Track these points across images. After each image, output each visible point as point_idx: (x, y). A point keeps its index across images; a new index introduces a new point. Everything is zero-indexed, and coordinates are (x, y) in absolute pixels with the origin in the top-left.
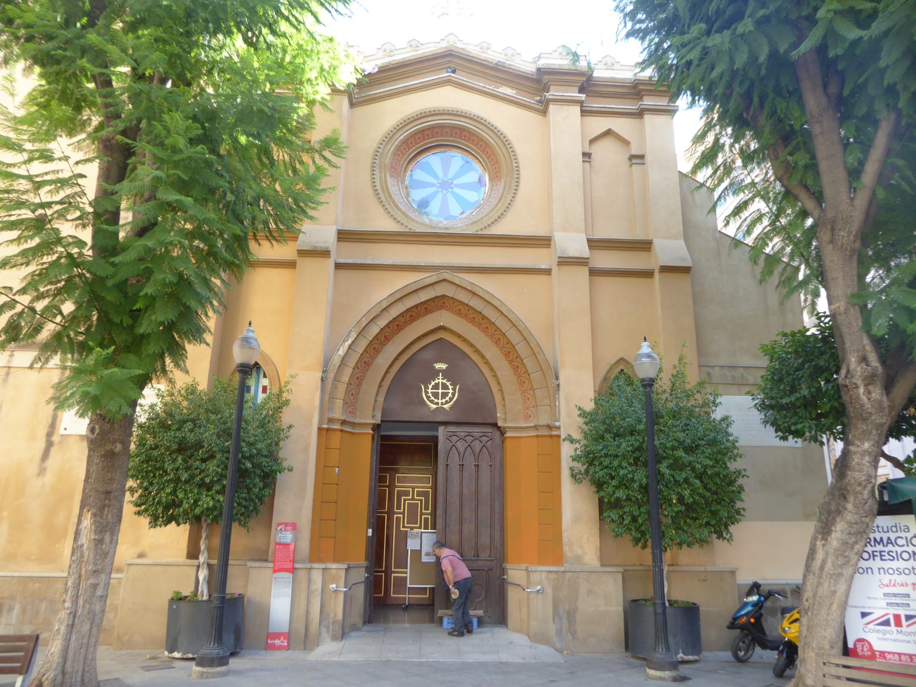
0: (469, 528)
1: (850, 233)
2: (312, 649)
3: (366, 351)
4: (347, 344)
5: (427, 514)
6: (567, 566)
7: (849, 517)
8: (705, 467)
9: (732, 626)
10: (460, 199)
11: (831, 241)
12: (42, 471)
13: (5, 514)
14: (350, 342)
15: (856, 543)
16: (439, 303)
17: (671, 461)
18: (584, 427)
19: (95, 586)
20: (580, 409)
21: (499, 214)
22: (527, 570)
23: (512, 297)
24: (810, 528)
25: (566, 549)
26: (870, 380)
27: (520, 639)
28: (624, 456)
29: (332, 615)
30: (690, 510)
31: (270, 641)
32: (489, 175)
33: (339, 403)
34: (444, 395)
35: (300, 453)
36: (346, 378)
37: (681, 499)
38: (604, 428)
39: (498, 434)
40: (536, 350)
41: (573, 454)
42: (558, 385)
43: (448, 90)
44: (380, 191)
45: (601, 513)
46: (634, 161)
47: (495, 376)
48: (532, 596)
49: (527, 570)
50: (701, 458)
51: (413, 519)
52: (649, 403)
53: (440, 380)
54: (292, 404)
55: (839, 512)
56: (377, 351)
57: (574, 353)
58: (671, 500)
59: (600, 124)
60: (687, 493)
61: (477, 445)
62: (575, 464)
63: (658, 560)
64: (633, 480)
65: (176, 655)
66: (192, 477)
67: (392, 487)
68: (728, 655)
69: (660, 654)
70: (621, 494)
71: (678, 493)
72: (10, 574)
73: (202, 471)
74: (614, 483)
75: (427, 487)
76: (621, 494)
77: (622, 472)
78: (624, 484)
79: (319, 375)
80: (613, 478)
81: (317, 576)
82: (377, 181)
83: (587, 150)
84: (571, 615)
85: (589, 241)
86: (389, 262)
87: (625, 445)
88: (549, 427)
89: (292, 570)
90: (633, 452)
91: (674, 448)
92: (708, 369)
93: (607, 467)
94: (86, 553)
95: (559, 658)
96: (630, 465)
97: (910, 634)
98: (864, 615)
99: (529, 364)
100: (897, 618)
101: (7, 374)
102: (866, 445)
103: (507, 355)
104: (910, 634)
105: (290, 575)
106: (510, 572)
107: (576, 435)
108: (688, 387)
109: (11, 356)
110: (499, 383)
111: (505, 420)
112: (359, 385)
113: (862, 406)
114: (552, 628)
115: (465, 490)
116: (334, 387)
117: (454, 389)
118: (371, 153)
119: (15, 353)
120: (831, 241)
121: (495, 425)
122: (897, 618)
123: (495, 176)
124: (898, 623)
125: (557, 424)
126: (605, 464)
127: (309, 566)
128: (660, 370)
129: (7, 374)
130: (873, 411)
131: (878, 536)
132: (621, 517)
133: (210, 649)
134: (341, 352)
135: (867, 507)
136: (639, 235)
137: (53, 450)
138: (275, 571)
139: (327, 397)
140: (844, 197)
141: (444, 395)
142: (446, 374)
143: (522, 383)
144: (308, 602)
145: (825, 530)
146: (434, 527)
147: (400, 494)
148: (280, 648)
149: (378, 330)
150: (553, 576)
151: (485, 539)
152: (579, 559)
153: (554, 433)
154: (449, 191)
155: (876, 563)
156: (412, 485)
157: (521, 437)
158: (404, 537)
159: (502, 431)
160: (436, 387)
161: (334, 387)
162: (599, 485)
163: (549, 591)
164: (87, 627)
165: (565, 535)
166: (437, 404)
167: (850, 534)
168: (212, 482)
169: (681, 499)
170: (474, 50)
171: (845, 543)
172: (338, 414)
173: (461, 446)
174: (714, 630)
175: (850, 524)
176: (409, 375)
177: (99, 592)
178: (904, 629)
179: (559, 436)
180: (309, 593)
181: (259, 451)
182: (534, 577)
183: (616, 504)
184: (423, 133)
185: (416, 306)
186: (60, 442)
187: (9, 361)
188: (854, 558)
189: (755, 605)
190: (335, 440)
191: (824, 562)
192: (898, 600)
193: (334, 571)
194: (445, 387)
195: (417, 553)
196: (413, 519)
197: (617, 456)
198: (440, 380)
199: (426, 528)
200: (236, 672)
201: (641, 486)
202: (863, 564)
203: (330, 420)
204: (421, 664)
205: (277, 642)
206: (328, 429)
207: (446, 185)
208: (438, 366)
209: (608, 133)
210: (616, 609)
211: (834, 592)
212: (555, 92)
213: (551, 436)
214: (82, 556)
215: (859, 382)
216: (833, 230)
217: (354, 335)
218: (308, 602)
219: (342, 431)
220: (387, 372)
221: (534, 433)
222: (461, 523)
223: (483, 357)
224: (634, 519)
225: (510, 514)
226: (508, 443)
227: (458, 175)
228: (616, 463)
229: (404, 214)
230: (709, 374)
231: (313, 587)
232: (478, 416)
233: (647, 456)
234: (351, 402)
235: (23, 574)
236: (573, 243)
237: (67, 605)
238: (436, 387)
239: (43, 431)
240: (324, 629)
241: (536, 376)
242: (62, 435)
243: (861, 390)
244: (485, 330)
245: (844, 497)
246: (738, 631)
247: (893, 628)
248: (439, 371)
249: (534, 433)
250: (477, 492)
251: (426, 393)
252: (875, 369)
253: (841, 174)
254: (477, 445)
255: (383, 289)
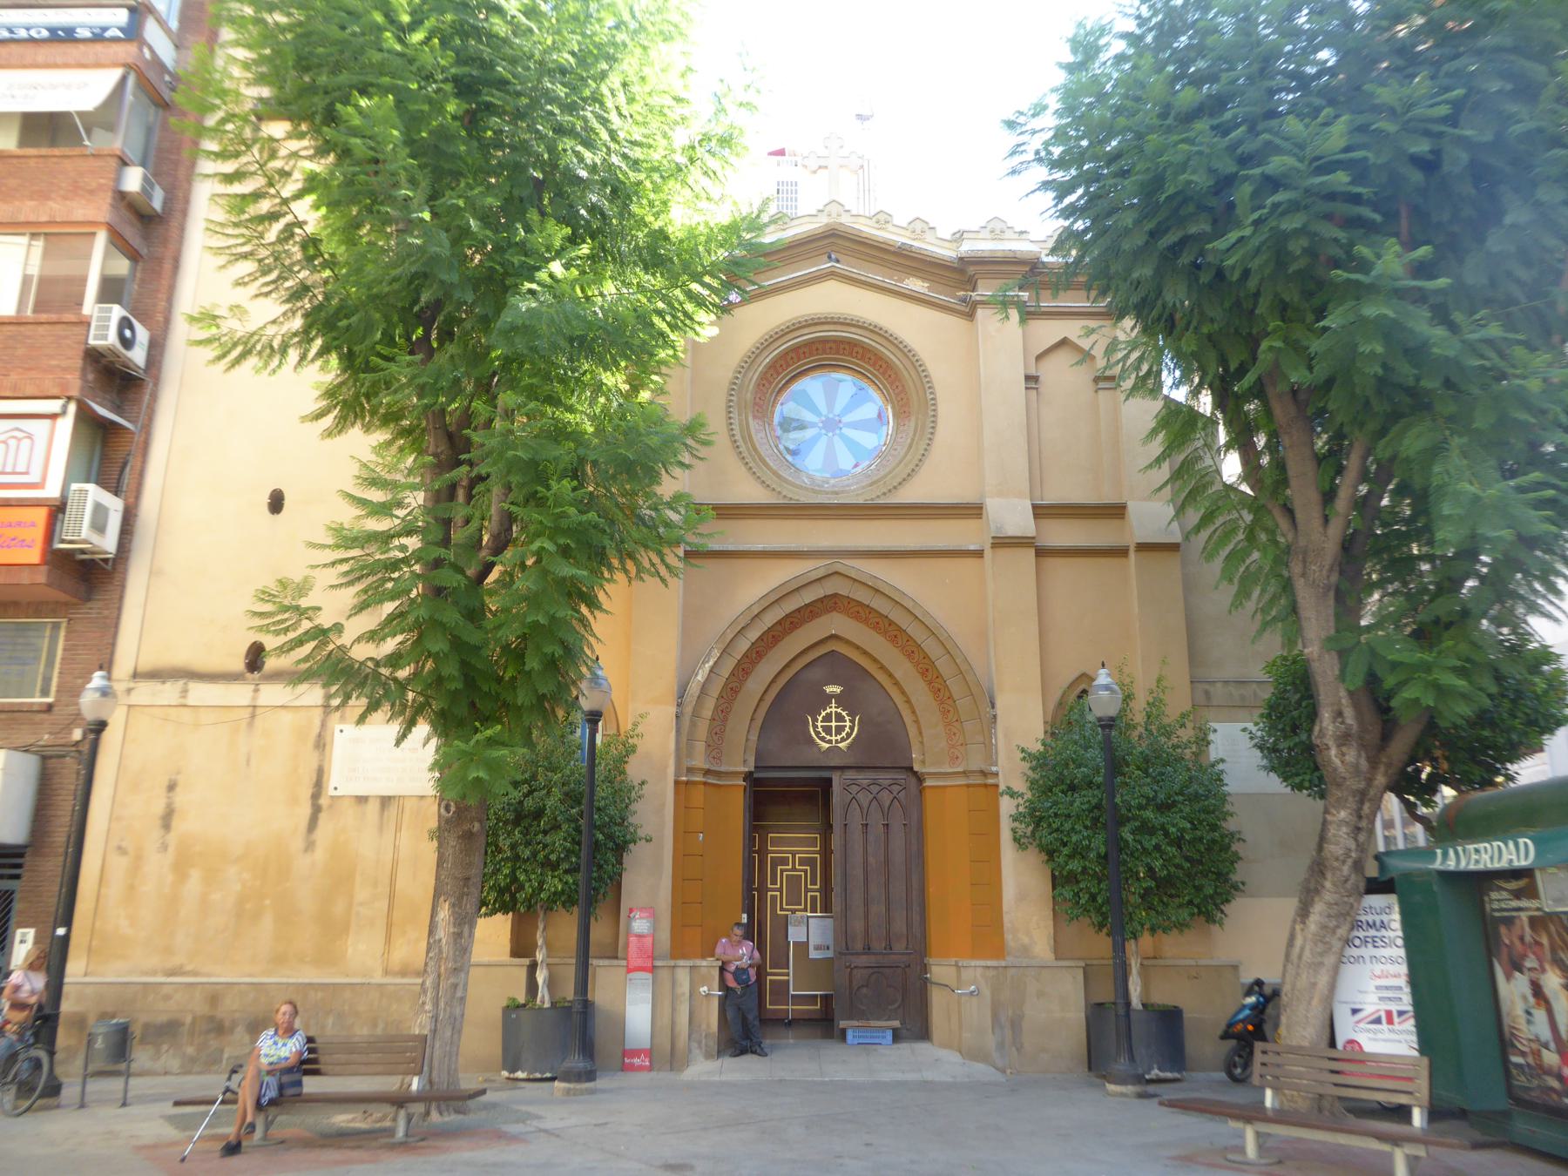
0: (878, 909)
1: (1321, 567)
2: (681, 1070)
3: (732, 674)
4: (708, 666)
5: (815, 891)
6: (1010, 960)
7: (1328, 897)
8: (1183, 830)
9: (1226, 1036)
10: (852, 445)
11: (1303, 575)
12: (310, 846)
13: (267, 902)
14: (711, 663)
15: (1338, 927)
16: (831, 603)
17: (1137, 824)
18: (1030, 773)
19: (455, 986)
20: (1023, 751)
21: (912, 466)
22: (956, 965)
23: (926, 591)
24: (1291, 905)
25: (1008, 937)
26: (1344, 739)
27: (951, 1057)
28: (1078, 817)
29: (704, 1026)
30: (1164, 886)
31: (625, 1060)
32: (893, 408)
33: (700, 747)
34: (839, 730)
35: (655, 814)
36: (707, 712)
37: (1151, 871)
38: (1054, 777)
39: (913, 780)
40: (964, 667)
41: (1014, 812)
42: (995, 716)
43: (831, 286)
44: (740, 443)
45: (1054, 888)
46: (1101, 385)
47: (908, 701)
48: (963, 999)
49: (956, 965)
50: (1177, 819)
51: (794, 899)
52: (1108, 746)
53: (833, 709)
54: (639, 749)
55: (1317, 891)
56: (747, 673)
57: (1017, 673)
58: (1137, 873)
59: (1050, 331)
60: (1158, 864)
61: (886, 797)
62: (1017, 824)
63: (1119, 950)
64: (1088, 847)
65: (520, 1075)
66: (535, 854)
67: (763, 852)
68: (1223, 1075)
69: (1122, 1065)
70: (1075, 865)
71: (1148, 865)
72: (284, 980)
73: (545, 846)
74: (1066, 851)
75: (813, 851)
76: (1075, 865)
77: (1074, 838)
78: (1078, 852)
79: (673, 710)
80: (1065, 845)
81: (683, 977)
82: (736, 427)
83: (1033, 372)
84: (1016, 1024)
85: (1035, 507)
86: (760, 547)
87: (1079, 802)
88: (984, 774)
89: (652, 969)
90: (1091, 811)
91: (1141, 807)
92: (1207, 687)
93: (1057, 830)
94: (445, 949)
95: (999, 1077)
96: (1086, 827)
97: (1401, 1032)
98: (1355, 1011)
99: (954, 686)
100: (1389, 1014)
101: (253, 716)
102: (1343, 814)
103: (924, 673)
104: (1401, 1032)
105: (649, 976)
106: (935, 969)
107: (1020, 786)
108: (1166, 721)
109: (256, 691)
110: (914, 712)
111: (923, 762)
112: (725, 720)
113: (1335, 769)
114: (990, 1041)
115: (871, 859)
116: (693, 724)
117: (852, 721)
118: (725, 385)
119: (262, 687)
120: (1303, 575)
121: (911, 769)
122: (1389, 1014)
123: (902, 413)
124: (1390, 1021)
125: (994, 769)
126: (1055, 826)
127: (672, 963)
128: (1128, 698)
129: (253, 716)
130: (1347, 775)
131: (1370, 918)
132: (1077, 895)
133: (576, 1062)
134: (700, 677)
135: (1349, 885)
136: (1108, 497)
137: (323, 816)
138: (629, 971)
139: (684, 740)
140: (1317, 523)
141: (839, 730)
142: (841, 700)
143: (945, 713)
144: (674, 1010)
145: (1304, 913)
146: (827, 908)
147: (776, 862)
148: (641, 1068)
149: (748, 645)
150: (991, 973)
151: (899, 926)
152: (1025, 950)
153: (991, 781)
154: (837, 435)
155: (1368, 951)
156: (793, 850)
157: (945, 787)
158: (784, 924)
159: (920, 779)
160: (828, 718)
161: (693, 724)
162: (1051, 854)
163: (987, 992)
164: (448, 1034)
165: (1006, 918)
166: (830, 742)
167: (1329, 916)
168: (559, 861)
169: (1151, 871)
170: (868, 229)
171: (1324, 927)
172: (700, 761)
173: (864, 798)
174: (1204, 1044)
175: (1329, 905)
176: (790, 705)
177: (459, 994)
178: (1396, 1027)
179: (997, 786)
180: (674, 999)
181: (611, 818)
182: (966, 975)
183: (1071, 878)
184: (799, 351)
185: (798, 610)
186: (330, 806)
187: (254, 698)
188: (1337, 945)
189: (1254, 1007)
190: (698, 796)
191: (1302, 949)
192: (1390, 994)
193: (704, 970)
194: (840, 718)
195: (803, 947)
196: (794, 899)
197: (1068, 816)
198: (833, 709)
199: (814, 910)
200: (603, 1091)
201: (1099, 856)
202: (1354, 952)
203: (690, 770)
204: (823, 1083)
205: (636, 1061)
206: (687, 783)
207: (832, 425)
208: (830, 689)
209: (1064, 342)
210: (1076, 1015)
211: (1314, 985)
212: (984, 291)
213: (986, 786)
214: (440, 951)
215: (1331, 743)
216: (1304, 561)
217: (716, 653)
218: (674, 1010)
219: (705, 784)
220: (761, 700)
221: (962, 781)
222: (866, 904)
223: (891, 676)
224: (1093, 898)
225: (932, 890)
226: (928, 795)
227: (848, 409)
228: (1067, 826)
229: (775, 473)
230: (1207, 693)
231: (679, 990)
232: (884, 752)
233: (1107, 817)
234: (716, 743)
235: (300, 980)
236: (1013, 516)
237: (428, 1007)
238: (828, 718)
239: (306, 792)
240: (694, 1045)
241: (963, 704)
242: (332, 797)
243: (1333, 752)
244: (893, 639)
245: (1323, 874)
246: (1233, 1042)
247: (1385, 1026)
248: (831, 696)
249: (962, 781)
250: (887, 861)
251: (815, 727)
252: (1349, 727)
253: (1314, 496)
254: (886, 797)
255: (754, 587)
